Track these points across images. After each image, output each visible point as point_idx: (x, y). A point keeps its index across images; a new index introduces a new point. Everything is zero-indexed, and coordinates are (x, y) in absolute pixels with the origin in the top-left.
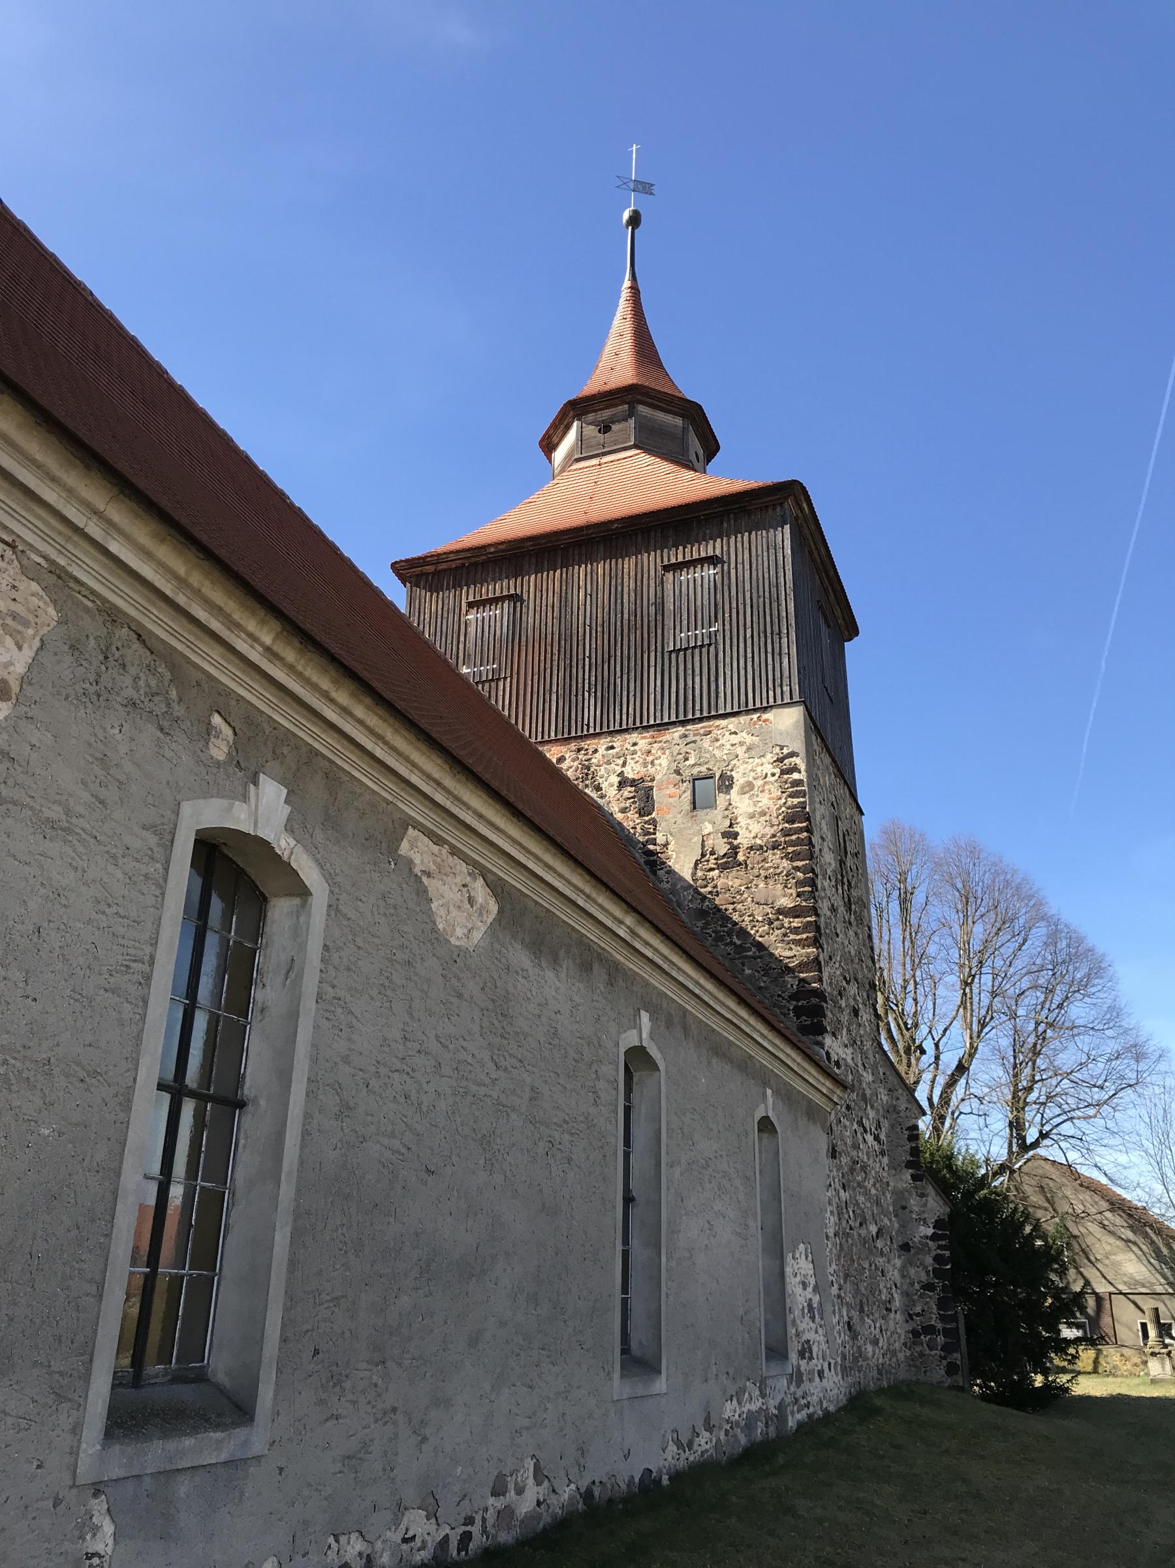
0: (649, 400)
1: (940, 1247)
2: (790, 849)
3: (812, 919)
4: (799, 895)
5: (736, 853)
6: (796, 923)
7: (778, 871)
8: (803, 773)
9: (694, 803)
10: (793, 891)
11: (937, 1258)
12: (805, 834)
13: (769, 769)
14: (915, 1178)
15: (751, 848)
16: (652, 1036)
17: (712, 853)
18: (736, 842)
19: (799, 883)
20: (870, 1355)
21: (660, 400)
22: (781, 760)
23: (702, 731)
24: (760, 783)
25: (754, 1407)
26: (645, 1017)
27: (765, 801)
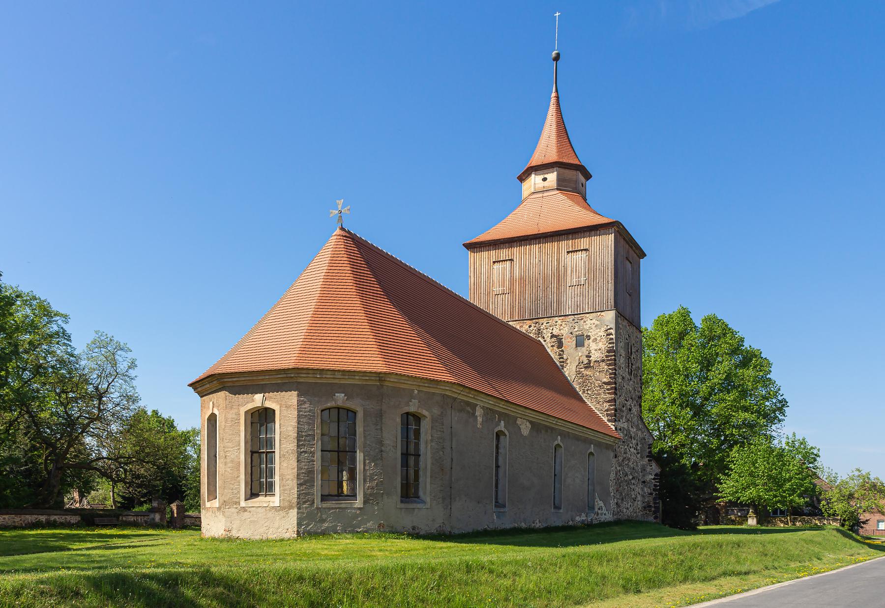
0: (563, 166)
1: (656, 482)
2: (608, 362)
3: (614, 386)
4: (610, 378)
5: (590, 363)
6: (609, 387)
7: (603, 369)
8: (614, 336)
9: (576, 344)
10: (608, 377)
11: (655, 485)
12: (613, 357)
13: (602, 334)
14: (649, 460)
15: (595, 361)
16: (560, 441)
17: (582, 363)
18: (590, 359)
19: (611, 374)
20: (625, 512)
21: (567, 165)
22: (607, 330)
23: (580, 319)
24: (599, 338)
25: (584, 519)
26: (559, 437)
27: (601, 345)
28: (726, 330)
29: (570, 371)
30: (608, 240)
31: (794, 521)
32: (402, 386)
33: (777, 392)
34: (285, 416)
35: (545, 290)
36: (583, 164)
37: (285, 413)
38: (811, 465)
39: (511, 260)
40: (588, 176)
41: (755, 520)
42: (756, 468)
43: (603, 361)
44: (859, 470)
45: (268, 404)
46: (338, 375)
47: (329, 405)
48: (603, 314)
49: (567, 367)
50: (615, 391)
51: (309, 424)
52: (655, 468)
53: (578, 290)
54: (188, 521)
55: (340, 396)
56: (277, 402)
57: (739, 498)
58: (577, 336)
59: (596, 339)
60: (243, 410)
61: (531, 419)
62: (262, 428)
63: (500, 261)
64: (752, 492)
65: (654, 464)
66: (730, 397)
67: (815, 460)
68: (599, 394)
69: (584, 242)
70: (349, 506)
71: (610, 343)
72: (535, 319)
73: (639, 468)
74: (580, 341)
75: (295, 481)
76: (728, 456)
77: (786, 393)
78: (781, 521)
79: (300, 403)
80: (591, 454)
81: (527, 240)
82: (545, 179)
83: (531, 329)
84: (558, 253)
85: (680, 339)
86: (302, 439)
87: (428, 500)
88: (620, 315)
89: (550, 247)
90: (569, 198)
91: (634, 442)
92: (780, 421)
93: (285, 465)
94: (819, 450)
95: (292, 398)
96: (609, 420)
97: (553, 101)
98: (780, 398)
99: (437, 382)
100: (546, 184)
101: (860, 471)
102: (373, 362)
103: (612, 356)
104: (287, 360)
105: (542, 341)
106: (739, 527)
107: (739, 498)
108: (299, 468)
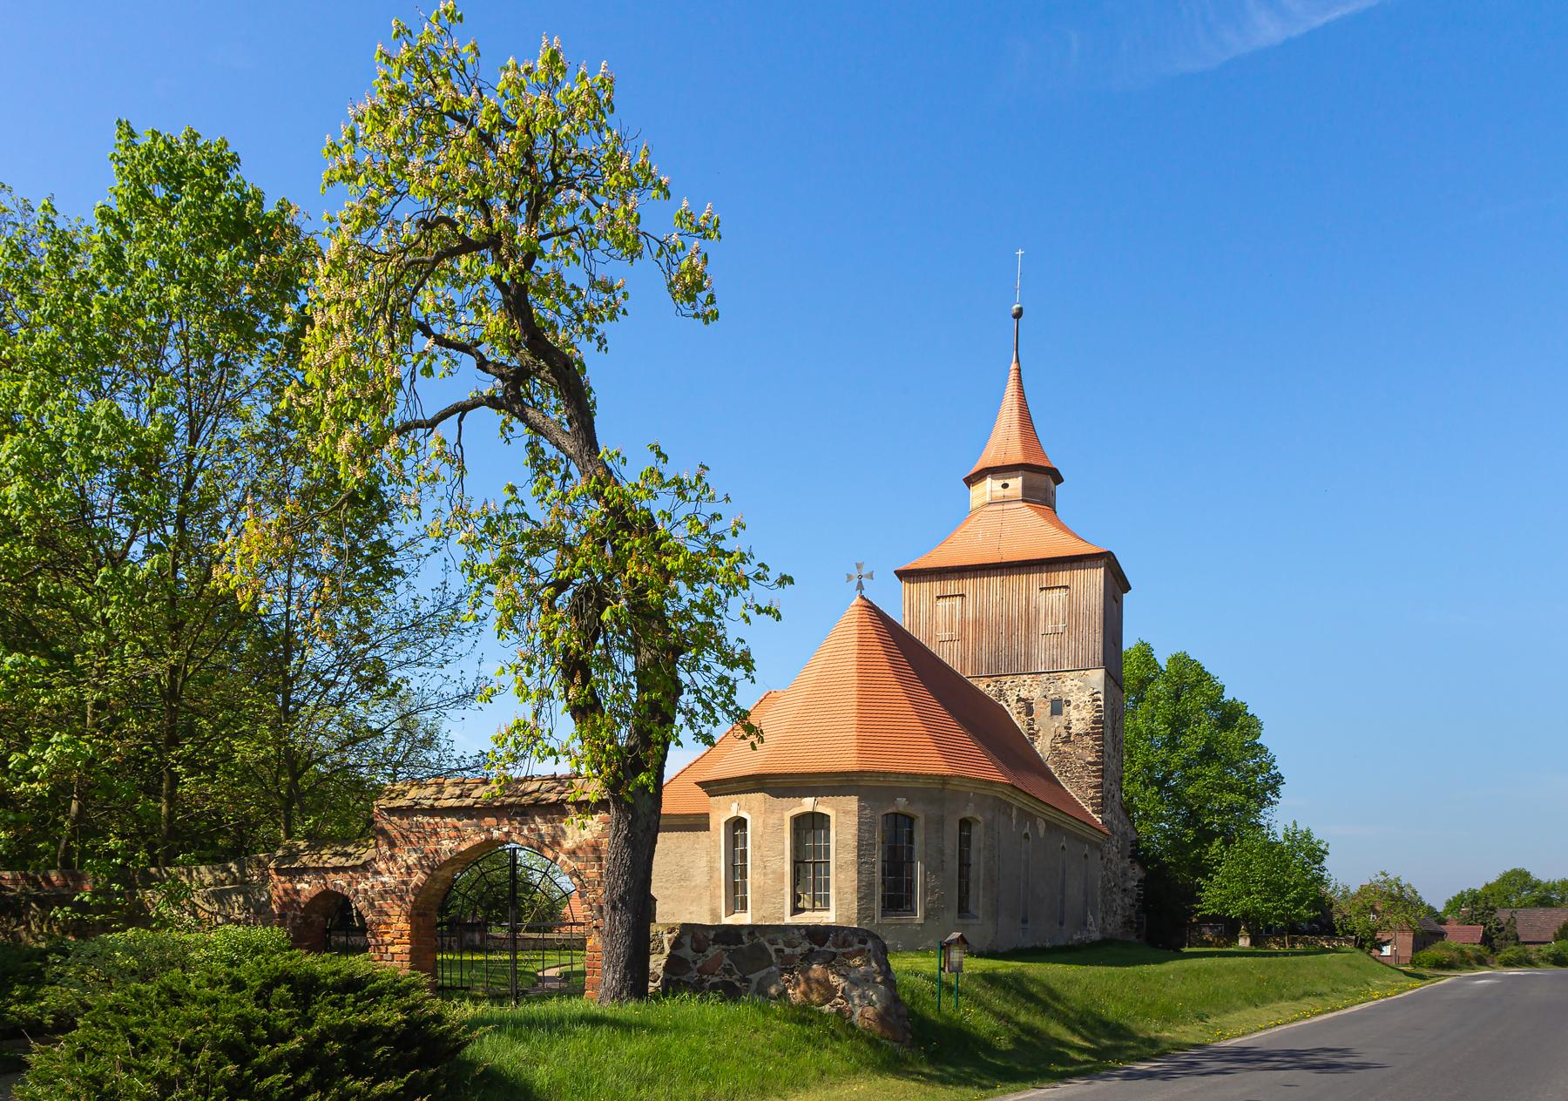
6: (1094, 768)
13: (1087, 699)
15: (1077, 735)
19: (1097, 751)
24: (1082, 705)
27: (1084, 714)
28: (1203, 676)
29: (1042, 746)
30: (1097, 575)
31: (1293, 942)
32: (961, 789)
33: (1270, 764)
34: (842, 823)
35: (1009, 637)
36: (1054, 466)
37: (842, 819)
38: (1317, 866)
39: (963, 596)
40: (1058, 479)
41: (1248, 940)
42: (1251, 871)
43: (1087, 734)
44: (1383, 874)
45: (820, 809)
46: (902, 778)
47: (890, 811)
48: (1087, 672)
49: (1039, 741)
50: (1103, 773)
51: (869, 832)
52: (1138, 872)
53: (1054, 640)
54: (491, 943)
55: (902, 801)
56: (832, 807)
57: (1227, 910)
58: (1052, 701)
59: (1078, 706)
60: (788, 815)
61: (1047, 818)
62: (808, 836)
63: (946, 597)
64: (1245, 903)
65: (1137, 867)
66: (1212, 771)
67: (1323, 859)
68: (1082, 777)
69: (1063, 577)
70: (909, 921)
71: (1097, 712)
72: (995, 676)
73: (1119, 872)
74: (1057, 707)
75: (855, 895)
76: (1207, 853)
77: (1281, 767)
78: (1275, 942)
79: (861, 809)
80: (1086, 856)
81: (984, 569)
82: (1005, 486)
83: (990, 689)
84: (1028, 588)
85: (1141, 688)
86: (863, 848)
87: (980, 914)
88: (1108, 674)
89: (1018, 581)
90: (1039, 514)
91: (1116, 838)
92: (1272, 803)
93: (843, 877)
94: (1327, 845)
95: (852, 803)
96: (1094, 812)
97: (1013, 374)
98: (1273, 772)
99: (992, 783)
100: (1007, 492)
101: (1386, 875)
102: (933, 763)
103: (1099, 728)
104: (847, 760)
105: (1005, 705)
106: (1227, 949)
107: (1227, 910)
108: (860, 881)
